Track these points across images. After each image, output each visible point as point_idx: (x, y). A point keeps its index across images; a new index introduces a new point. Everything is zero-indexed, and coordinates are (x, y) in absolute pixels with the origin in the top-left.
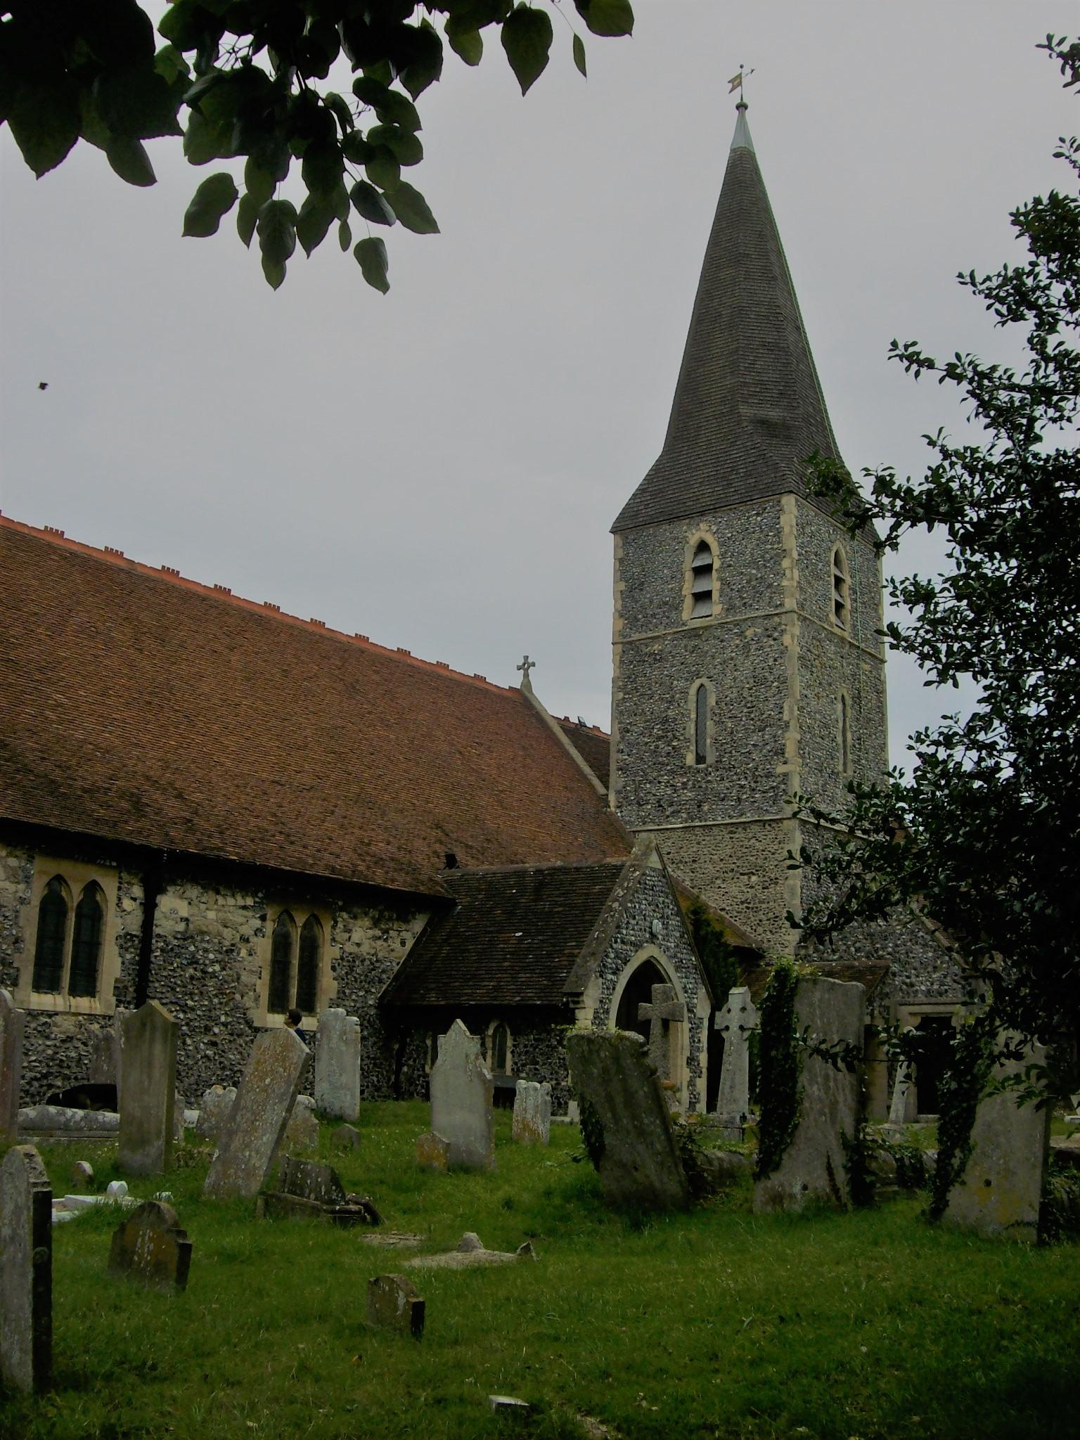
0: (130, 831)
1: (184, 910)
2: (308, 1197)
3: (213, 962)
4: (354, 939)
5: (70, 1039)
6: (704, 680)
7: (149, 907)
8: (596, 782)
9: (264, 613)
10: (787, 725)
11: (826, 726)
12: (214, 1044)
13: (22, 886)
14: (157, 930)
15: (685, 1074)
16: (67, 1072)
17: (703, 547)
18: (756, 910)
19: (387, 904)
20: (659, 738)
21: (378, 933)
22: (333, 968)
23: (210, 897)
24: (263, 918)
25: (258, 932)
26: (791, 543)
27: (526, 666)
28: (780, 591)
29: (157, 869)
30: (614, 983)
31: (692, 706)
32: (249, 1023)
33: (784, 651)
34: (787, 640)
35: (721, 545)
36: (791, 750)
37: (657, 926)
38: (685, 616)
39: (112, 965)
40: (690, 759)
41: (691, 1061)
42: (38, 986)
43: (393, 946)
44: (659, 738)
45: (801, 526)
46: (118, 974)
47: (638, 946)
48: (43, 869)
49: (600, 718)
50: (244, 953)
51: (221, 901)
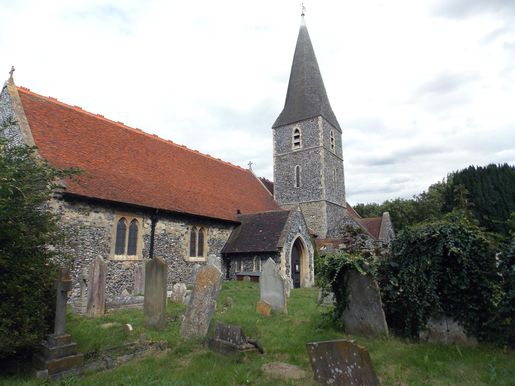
0: (146, 203)
1: (164, 227)
2: (229, 341)
3: (173, 242)
4: (214, 234)
5: (128, 269)
6: (298, 165)
7: (153, 226)
8: (270, 193)
9: (182, 148)
10: (321, 176)
11: (331, 177)
12: (174, 267)
13: (111, 221)
14: (155, 233)
15: (308, 270)
16: (127, 279)
17: (297, 131)
18: (315, 225)
19: (222, 224)
20: (287, 181)
21: (220, 232)
22: (208, 243)
23: (172, 223)
24: (188, 229)
25: (186, 233)
26: (321, 128)
27: (250, 164)
28: (318, 141)
29: (155, 214)
30: (290, 244)
31: (295, 172)
32: (184, 260)
33: (320, 157)
34: (321, 154)
35: (302, 130)
36: (323, 183)
37: (300, 227)
38: (293, 149)
39: (141, 245)
40: (295, 186)
41: (310, 266)
42: (117, 253)
43: (224, 236)
44: (287, 181)
45: (324, 124)
46: (144, 247)
47: (296, 233)
48: (117, 218)
49: (271, 179)
50: (182, 239)
51: (175, 224)
